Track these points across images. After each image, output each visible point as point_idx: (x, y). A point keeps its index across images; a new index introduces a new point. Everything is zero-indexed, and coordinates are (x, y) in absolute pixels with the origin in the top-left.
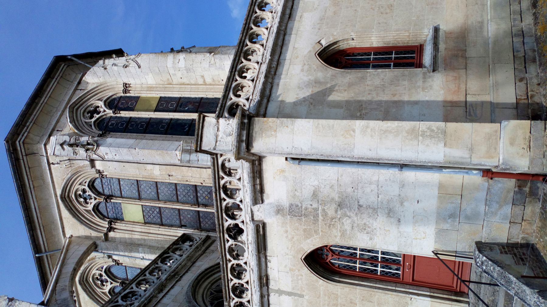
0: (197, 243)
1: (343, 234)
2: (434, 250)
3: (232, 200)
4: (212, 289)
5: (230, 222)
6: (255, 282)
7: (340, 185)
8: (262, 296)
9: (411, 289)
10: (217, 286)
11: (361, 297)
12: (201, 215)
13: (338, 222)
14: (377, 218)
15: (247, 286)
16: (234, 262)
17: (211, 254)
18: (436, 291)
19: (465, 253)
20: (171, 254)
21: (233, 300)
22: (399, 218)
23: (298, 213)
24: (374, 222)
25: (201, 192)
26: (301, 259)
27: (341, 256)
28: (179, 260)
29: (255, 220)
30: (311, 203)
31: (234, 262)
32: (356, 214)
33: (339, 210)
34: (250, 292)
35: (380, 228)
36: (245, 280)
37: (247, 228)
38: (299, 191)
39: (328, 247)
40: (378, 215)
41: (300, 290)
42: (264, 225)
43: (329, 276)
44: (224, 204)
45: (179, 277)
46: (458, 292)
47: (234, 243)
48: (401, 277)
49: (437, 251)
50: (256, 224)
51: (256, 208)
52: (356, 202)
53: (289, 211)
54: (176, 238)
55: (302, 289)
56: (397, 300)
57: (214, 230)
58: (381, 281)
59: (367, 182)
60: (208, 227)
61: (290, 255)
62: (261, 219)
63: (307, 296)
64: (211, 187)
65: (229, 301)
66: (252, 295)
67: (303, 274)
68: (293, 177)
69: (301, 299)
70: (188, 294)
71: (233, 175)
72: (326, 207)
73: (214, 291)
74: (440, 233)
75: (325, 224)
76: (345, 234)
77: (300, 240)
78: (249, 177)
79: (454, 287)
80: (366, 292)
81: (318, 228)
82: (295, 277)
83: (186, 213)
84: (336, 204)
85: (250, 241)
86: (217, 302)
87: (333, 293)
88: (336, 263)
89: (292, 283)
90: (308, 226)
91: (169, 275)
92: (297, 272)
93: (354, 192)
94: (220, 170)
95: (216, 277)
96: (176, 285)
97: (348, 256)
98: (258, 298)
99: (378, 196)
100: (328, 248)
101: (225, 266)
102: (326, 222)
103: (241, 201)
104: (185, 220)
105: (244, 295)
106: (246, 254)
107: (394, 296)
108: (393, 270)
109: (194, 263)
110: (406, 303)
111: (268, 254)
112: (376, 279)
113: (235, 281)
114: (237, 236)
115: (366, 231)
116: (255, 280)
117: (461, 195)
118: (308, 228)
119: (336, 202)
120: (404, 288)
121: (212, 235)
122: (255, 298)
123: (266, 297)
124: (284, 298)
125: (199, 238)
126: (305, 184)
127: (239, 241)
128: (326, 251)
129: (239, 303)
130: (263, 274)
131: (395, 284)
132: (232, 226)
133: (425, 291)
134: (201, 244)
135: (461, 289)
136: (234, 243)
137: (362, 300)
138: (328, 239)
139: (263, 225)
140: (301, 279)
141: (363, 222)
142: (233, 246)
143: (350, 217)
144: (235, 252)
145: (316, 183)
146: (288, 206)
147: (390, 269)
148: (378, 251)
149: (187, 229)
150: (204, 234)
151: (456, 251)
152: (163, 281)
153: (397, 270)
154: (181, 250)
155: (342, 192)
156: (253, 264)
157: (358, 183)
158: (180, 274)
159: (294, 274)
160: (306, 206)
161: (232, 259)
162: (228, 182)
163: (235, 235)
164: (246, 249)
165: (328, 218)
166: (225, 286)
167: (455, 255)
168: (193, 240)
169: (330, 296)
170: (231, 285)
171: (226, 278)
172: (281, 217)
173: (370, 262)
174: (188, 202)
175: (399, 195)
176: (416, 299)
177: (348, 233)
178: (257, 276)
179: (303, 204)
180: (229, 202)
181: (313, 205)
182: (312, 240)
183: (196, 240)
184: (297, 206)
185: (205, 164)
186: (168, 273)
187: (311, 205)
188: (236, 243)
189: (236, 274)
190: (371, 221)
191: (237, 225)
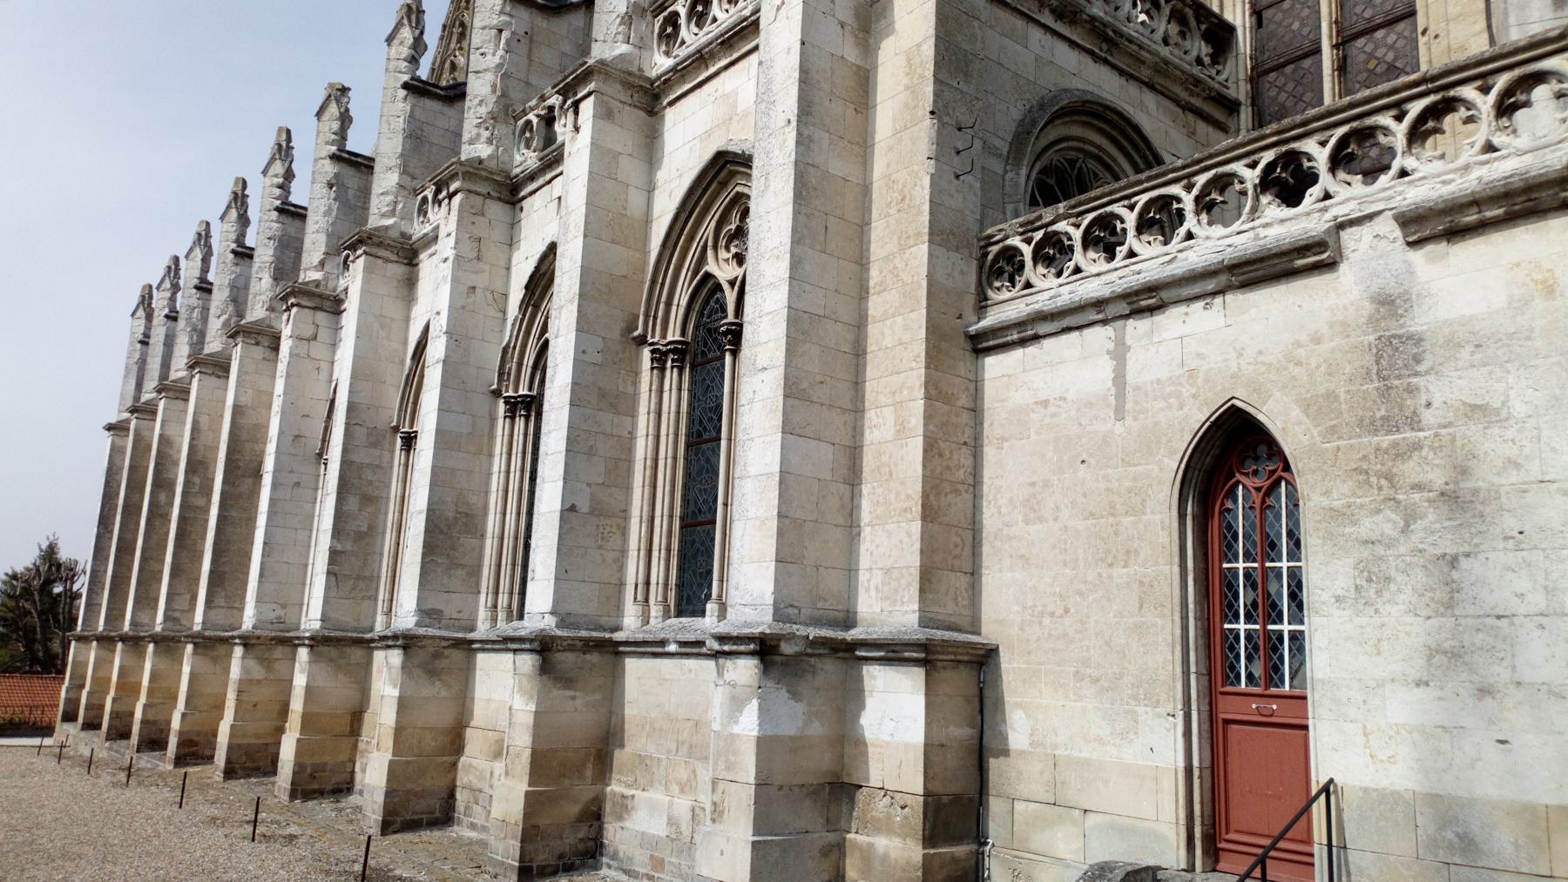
0: (1210, 77)
1: (1337, 515)
2: (1339, 786)
3: (1405, 141)
4: (1083, 162)
5: (1318, 152)
6: (1137, 276)
7: (1525, 492)
8: (1099, 304)
9: (1199, 714)
10: (1094, 172)
11: (1148, 579)
12: (1307, 63)
13: (1378, 495)
14: (1417, 615)
15: (1119, 256)
16: (1188, 202)
17: (1185, 130)
18: (1208, 784)
19: (1344, 873)
20: (1167, 10)
21: (1074, 225)
22: (1431, 684)
23: (1392, 366)
24: (1402, 607)
25: (1392, 38)
26: (1233, 398)
27: (1261, 514)
28: (1151, 40)
29: (1342, 234)
30: (1436, 404)
31: (1188, 202)
32: (1420, 551)
33: (1426, 494)
34: (1106, 267)
35: (1383, 625)
36: (1137, 247)
37: (1308, 214)
38: (1478, 356)
39: (1285, 475)
40: (1429, 618)
41: (1138, 408)
42: (1330, 266)
43: (1193, 485)
44: (1385, 120)
45: (1103, 55)
46: (1215, 845)
47: (1249, 186)
48: (1229, 689)
49: (1335, 791)
50: (1328, 239)
51: (1387, 227)
52: (1466, 548)
53: (1394, 336)
54: (1216, 9)
55: (1141, 412)
56: (1161, 678)
57: (1259, 121)
58: (1207, 632)
59: (1554, 576)
60: (1268, 97)
61: (1239, 364)
62: (1346, 252)
63: (1122, 430)
64: (1417, 67)
65: (1071, 216)
66: (1098, 275)
67: (1186, 409)
68: (1532, 330)
69: (1112, 414)
70: (1064, 96)
71: (1505, 122)
72: (1431, 454)
73: (1081, 168)
74: (1383, 801)
75: (1364, 456)
76: (1340, 521)
77: (1294, 387)
78: (1506, 178)
79: (1227, 833)
80: (1167, 590)
81: (1345, 436)
82: (1173, 389)
83: (1306, 12)
84: (1447, 484)
85: (1262, 232)
86: (1052, 187)
87: (1144, 501)
88: (1235, 501)
89: (1152, 383)
90: (1346, 403)
91: (1105, 25)
92: (1187, 391)
93: (1506, 538)
94: (1517, 72)
95: (1119, 165)
96: (1083, 54)
97: (1265, 535)
98: (1092, 295)
99: (1502, 617)
100: (1279, 473)
101: (1170, 176)
102: (1372, 457)
103: (1403, 173)
104: (1279, 16)
105: (1041, 269)
106: (1218, 230)
107: (1171, 668)
108: (1246, 667)
109: (1151, 87)
110: (1158, 701)
111: (1229, 297)
112: (1209, 619)
113: (1131, 219)
114: (1274, 190)
115: (1365, 584)
116: (1142, 275)
117: (1551, 877)
118: (1340, 404)
119: (1456, 483)
120: (1198, 696)
121: (1243, 116)
122: (1092, 285)
123: (1100, 316)
124: (1106, 368)
125: (1226, 81)
126: (1508, 372)
127: (1257, 199)
128: (1271, 468)
129: (1069, 243)
130: (1165, 295)
131: (1205, 672)
132: (1306, 164)
133: (1200, 755)
134: (1211, 89)
135: (1225, 853)
136: (1249, 186)
137: (1141, 583)
138: (1314, 472)
139: (1326, 262)
140: (1169, 407)
141: (1393, 573)
142: (1238, 187)
143: (1405, 530)
144: (1221, 195)
145: (1519, 409)
146: (1412, 329)
147: (1249, 658)
148: (1302, 622)
149: (1251, 32)
150: (1241, 91)
151: (1345, 847)
152: (1087, 11)
153: (1250, 677)
154: (1182, 34)
155: (1499, 498)
156: (1190, 260)
157: (1544, 550)
158: (1111, 55)
159: (1180, 384)
160: (1423, 389)
161: (1195, 192)
162: (1470, 113)
163: (1279, 182)
164: (1236, 226)
165: (1390, 464)
166: (1110, 193)
167: (1334, 842)
168: (1218, 63)
169: (1136, 494)
170: (1117, 209)
171: (1136, 189)
172: (1365, 313)
173: (1260, 601)
174: (1346, 9)
175: (1519, 684)
176: (1175, 728)
177: (1347, 530)
178: (1156, 277)
179: (1428, 377)
180: (1394, 135)
181: (1430, 411)
182: (1300, 423)
183: (1218, 72)
184: (1418, 359)
185: (1512, 20)
186: (1111, 20)
187: (1429, 405)
188: (1250, 192)
189: (1152, 215)
190: (1402, 596)
191: (1312, 179)
